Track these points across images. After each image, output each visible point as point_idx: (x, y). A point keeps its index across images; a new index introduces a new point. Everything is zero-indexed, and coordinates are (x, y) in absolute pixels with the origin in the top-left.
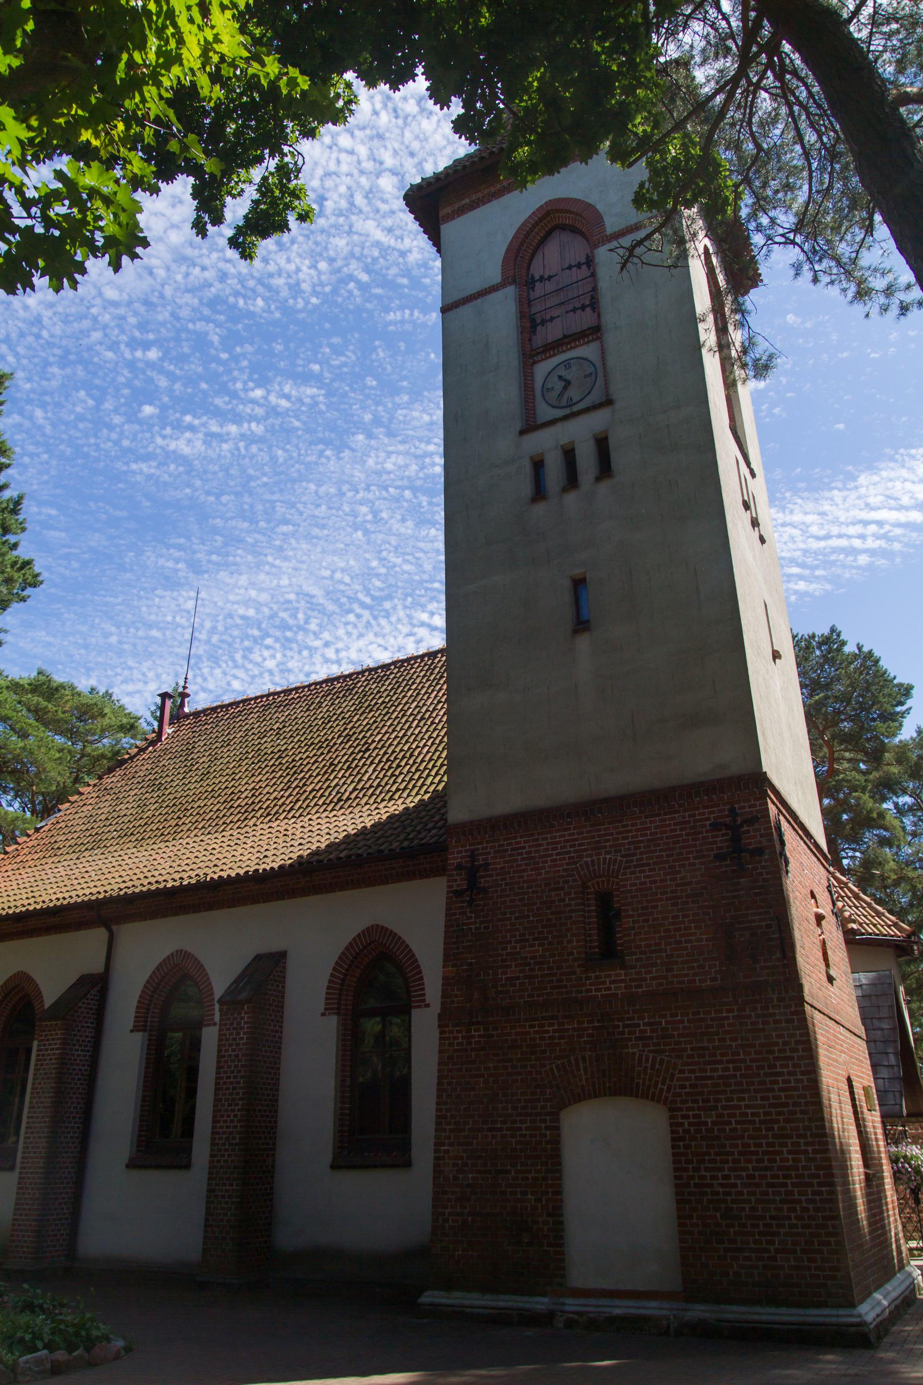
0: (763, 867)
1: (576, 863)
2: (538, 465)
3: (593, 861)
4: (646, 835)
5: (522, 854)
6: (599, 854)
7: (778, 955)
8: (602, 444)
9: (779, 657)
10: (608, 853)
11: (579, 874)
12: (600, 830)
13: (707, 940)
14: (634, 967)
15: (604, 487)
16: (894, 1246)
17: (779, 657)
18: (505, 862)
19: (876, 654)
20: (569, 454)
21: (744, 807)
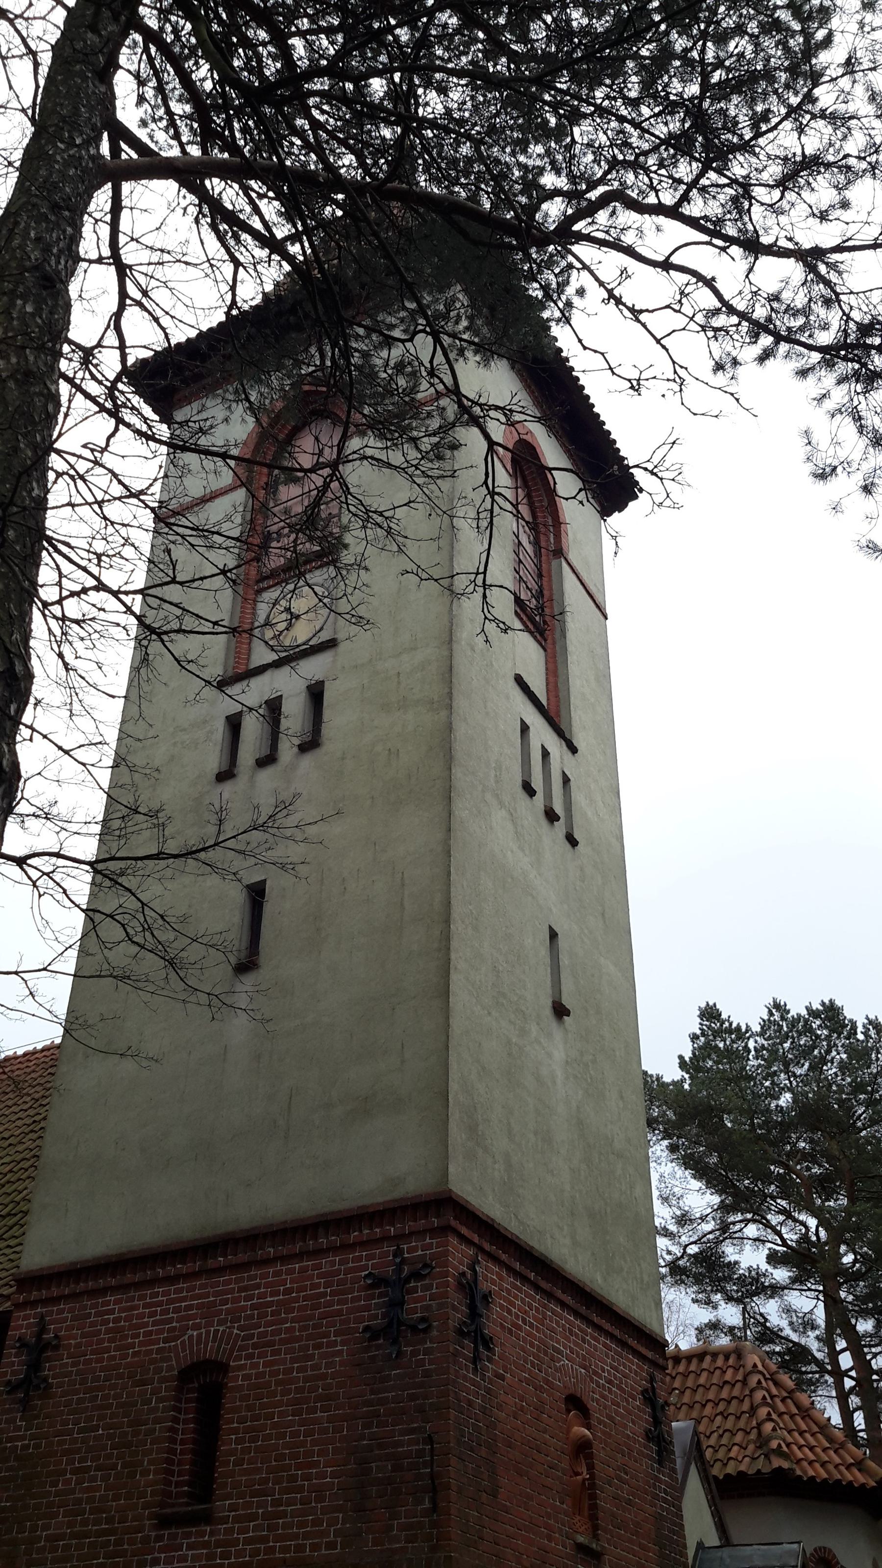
0: (427, 1352)
1: (175, 1339)
2: (234, 724)
3: (199, 1336)
4: (277, 1293)
5: (107, 1322)
6: (209, 1324)
7: (427, 1504)
8: (316, 694)
9: (567, 1013)
10: (221, 1323)
11: (177, 1355)
12: (218, 1284)
13: (333, 1475)
14: (225, 1520)
15: (308, 761)
16: (504, 1257)
17: (567, 1013)
18: (83, 1336)
19: (839, 1003)
20: (274, 707)
21: (415, 1249)
